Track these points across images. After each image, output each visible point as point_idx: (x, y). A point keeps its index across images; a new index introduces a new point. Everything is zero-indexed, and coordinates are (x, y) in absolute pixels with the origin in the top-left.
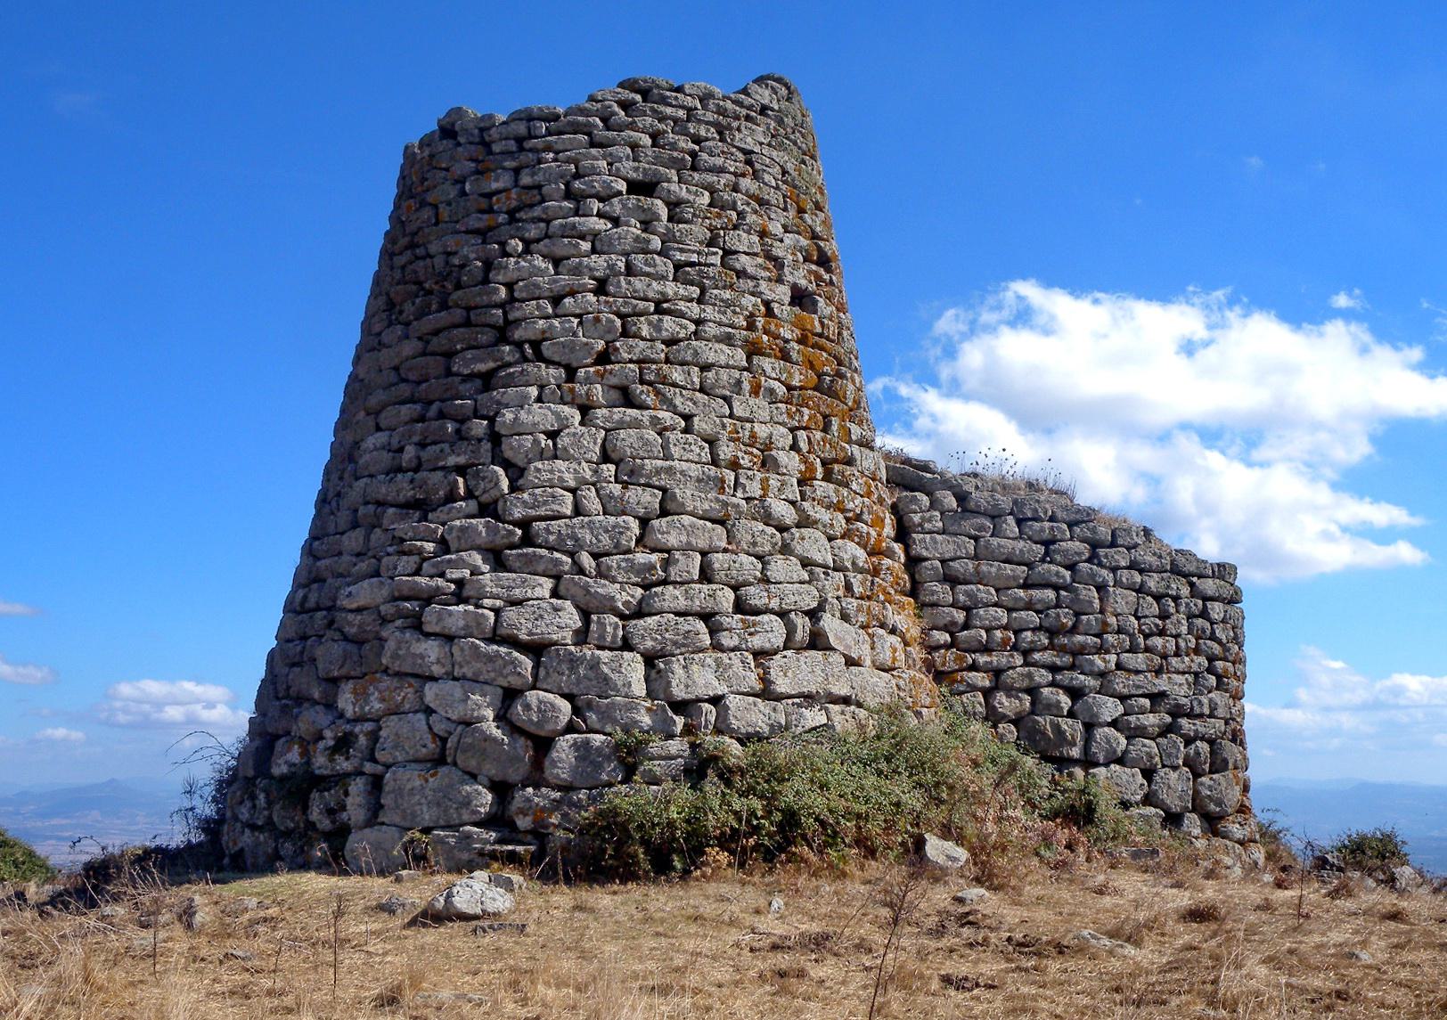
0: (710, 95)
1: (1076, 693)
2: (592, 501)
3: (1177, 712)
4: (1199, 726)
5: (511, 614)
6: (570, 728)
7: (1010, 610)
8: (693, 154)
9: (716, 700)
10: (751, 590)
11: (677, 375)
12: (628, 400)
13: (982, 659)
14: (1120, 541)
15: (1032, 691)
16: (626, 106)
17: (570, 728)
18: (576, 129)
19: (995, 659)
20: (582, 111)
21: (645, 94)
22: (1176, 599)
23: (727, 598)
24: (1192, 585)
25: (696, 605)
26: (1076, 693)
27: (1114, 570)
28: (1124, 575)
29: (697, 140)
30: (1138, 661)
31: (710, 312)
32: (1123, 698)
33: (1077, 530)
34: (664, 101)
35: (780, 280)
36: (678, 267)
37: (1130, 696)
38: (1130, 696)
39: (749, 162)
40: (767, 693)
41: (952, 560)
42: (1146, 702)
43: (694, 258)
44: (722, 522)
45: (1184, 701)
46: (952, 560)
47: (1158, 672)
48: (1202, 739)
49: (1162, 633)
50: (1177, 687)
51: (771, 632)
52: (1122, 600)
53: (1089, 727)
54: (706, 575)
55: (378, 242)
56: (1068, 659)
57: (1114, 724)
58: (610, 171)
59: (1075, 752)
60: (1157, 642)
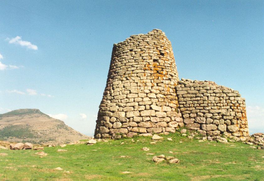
0: (142, 35)
1: (204, 113)
2: (121, 93)
3: (223, 115)
4: (227, 117)
5: (111, 108)
6: (116, 121)
7: (193, 101)
8: (138, 44)
9: (133, 117)
10: (140, 102)
11: (133, 75)
12: (127, 79)
13: (188, 109)
14: (211, 89)
15: (197, 113)
16: (130, 40)
17: (116, 121)
18: (124, 44)
19: (191, 109)
20: (125, 42)
21: (133, 37)
22: (223, 97)
23: (137, 104)
24: (227, 95)
25: (132, 105)
26: (204, 113)
27: (210, 93)
28: (212, 94)
29: (139, 42)
30: (216, 107)
31: (138, 66)
32: (212, 114)
33: (204, 88)
34: (135, 38)
35: (151, 59)
36: (135, 60)
37: (214, 113)
38: (214, 113)
39: (148, 43)
40: (140, 116)
41: (183, 94)
42: (217, 114)
43: (137, 59)
44: (137, 94)
45: (224, 113)
46: (183, 94)
47: (219, 109)
48: (228, 119)
49: (220, 103)
50: (223, 111)
51: (143, 108)
52: (211, 98)
53: (206, 118)
54: (134, 101)
55: (112, 48)
56: (202, 108)
57: (211, 118)
58: (127, 49)
59: (204, 122)
60: (219, 104)
